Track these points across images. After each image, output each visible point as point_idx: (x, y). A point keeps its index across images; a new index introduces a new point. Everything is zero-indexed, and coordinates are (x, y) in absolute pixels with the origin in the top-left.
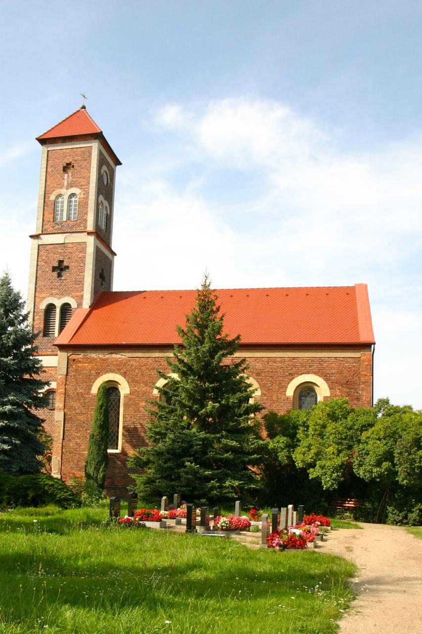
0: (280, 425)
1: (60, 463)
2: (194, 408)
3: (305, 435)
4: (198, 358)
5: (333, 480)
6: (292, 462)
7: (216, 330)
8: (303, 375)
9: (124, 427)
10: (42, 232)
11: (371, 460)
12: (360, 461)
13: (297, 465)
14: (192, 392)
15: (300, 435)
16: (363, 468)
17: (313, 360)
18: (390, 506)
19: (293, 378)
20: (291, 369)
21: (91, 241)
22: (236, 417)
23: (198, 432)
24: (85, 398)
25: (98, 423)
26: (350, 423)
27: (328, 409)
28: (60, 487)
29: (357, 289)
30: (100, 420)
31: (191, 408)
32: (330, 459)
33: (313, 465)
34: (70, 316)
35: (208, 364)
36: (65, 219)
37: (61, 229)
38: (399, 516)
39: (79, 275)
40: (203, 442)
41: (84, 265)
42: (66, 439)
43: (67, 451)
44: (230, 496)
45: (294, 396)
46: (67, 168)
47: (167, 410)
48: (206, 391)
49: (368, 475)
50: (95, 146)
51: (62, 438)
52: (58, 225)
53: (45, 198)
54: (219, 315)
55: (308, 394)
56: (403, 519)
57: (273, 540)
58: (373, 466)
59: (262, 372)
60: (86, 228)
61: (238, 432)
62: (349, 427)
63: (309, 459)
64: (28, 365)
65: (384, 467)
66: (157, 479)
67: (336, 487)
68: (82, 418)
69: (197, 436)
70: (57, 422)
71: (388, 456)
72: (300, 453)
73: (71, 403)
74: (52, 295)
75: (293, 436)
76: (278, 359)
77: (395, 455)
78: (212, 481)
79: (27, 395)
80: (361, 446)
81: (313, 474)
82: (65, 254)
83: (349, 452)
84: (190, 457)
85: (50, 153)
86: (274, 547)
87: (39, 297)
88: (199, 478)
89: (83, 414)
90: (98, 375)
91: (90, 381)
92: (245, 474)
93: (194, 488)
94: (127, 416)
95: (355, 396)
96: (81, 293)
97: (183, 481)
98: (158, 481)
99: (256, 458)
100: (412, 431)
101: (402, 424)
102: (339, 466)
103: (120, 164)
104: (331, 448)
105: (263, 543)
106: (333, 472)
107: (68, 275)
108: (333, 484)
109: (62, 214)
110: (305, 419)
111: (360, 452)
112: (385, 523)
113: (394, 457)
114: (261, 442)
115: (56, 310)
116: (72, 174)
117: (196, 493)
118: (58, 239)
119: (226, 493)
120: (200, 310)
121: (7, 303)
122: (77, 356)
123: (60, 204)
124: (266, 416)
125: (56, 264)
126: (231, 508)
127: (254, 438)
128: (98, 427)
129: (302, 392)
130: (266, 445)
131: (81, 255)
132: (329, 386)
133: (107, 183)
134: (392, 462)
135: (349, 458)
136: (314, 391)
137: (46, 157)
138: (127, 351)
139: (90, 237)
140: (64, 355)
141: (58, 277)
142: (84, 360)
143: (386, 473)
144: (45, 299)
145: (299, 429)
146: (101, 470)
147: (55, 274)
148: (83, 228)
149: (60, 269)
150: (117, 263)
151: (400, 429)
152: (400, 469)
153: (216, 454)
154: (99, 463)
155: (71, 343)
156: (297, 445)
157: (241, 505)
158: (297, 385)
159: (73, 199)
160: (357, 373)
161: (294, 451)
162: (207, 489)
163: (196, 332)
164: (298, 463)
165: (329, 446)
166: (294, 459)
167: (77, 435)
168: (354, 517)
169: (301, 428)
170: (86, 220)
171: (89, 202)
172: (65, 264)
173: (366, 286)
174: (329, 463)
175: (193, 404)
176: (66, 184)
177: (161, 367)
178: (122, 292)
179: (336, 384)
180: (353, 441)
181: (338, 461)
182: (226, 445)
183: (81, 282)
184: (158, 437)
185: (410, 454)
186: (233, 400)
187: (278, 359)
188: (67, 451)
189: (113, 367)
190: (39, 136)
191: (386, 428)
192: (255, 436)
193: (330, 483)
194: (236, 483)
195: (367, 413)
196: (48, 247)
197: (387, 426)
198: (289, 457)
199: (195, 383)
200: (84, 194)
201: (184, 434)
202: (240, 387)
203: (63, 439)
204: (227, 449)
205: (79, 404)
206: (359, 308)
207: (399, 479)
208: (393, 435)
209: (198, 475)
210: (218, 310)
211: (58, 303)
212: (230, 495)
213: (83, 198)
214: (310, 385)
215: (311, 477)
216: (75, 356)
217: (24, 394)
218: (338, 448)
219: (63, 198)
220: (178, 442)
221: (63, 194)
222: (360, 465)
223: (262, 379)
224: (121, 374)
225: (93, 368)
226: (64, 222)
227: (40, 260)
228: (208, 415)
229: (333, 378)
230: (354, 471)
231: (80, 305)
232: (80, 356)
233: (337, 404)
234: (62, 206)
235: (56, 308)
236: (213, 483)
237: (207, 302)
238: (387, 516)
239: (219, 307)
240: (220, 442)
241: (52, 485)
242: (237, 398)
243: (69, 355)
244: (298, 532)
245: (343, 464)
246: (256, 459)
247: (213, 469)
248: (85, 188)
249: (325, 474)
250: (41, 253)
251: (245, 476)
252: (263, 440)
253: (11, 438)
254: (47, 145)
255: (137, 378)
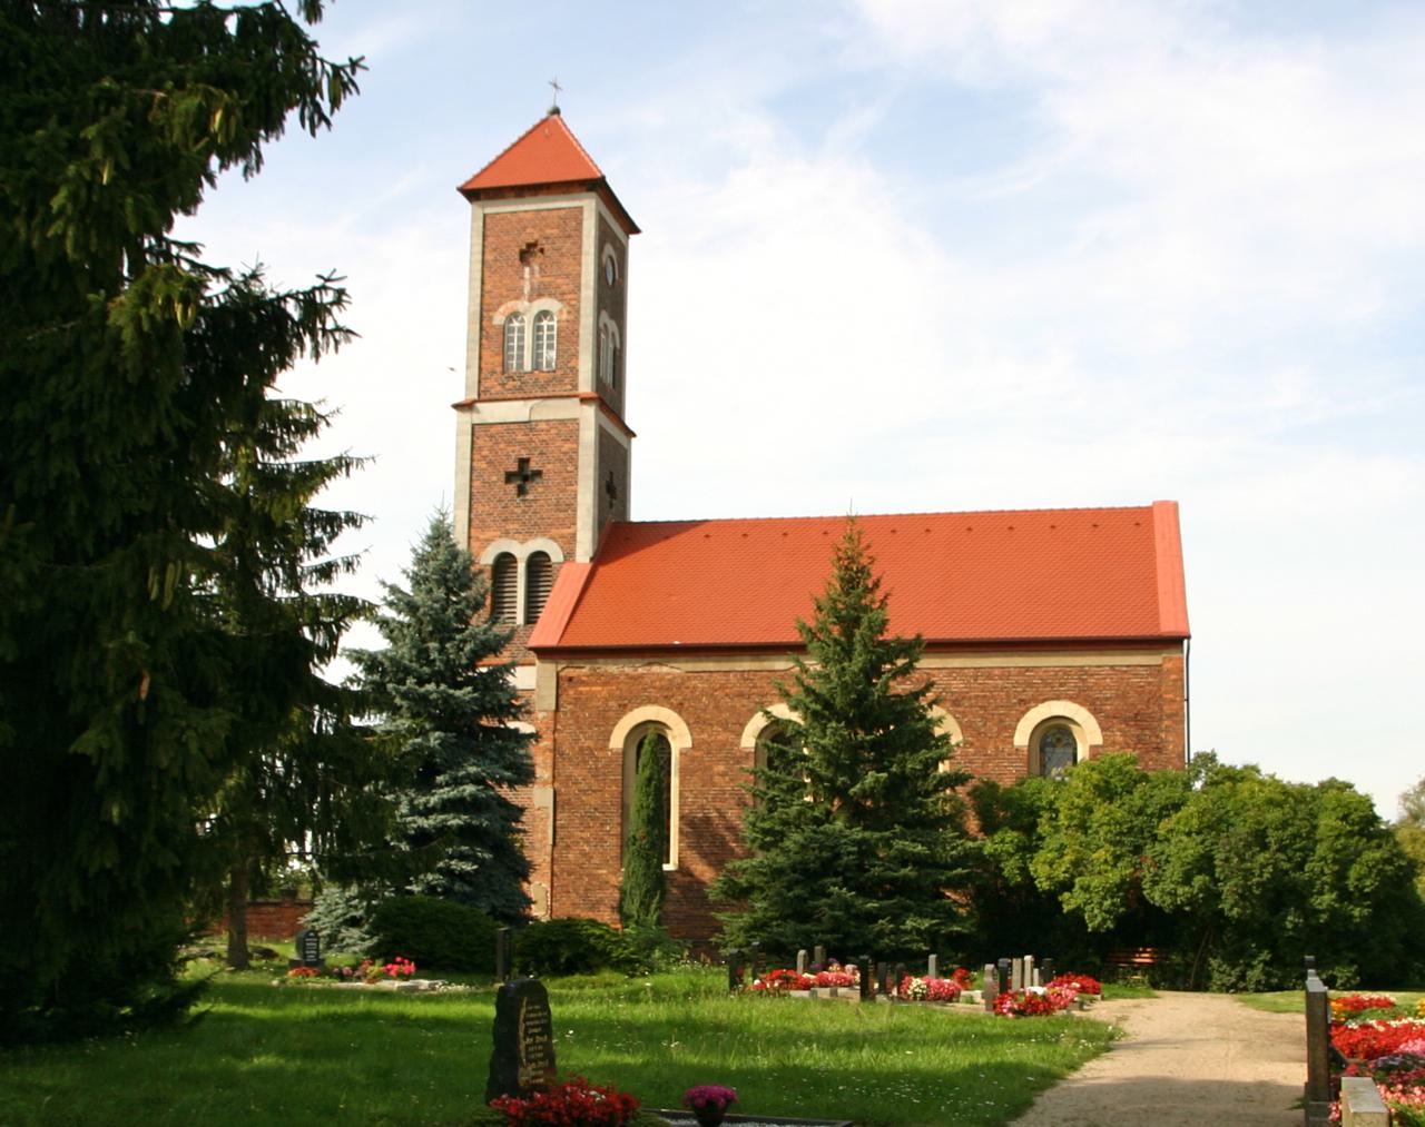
0: (1012, 812)
1: (549, 895)
2: (839, 783)
3: (1054, 827)
4: (845, 686)
5: (1106, 912)
6: (1030, 880)
7: (876, 629)
8: (1046, 704)
9: (682, 818)
10: (479, 395)
11: (1173, 871)
12: (1156, 875)
13: (1039, 886)
14: (834, 751)
15: (1044, 827)
16: (1161, 886)
17: (1067, 671)
18: (1215, 958)
19: (1028, 709)
20: (1024, 691)
21: (588, 417)
22: (920, 799)
23: (847, 828)
24: (597, 759)
25: (644, 813)
26: (1139, 803)
27: (1095, 776)
28: (614, 939)
29: (1157, 516)
30: (648, 807)
31: (832, 781)
32: (1099, 873)
33: (1067, 886)
34: (548, 589)
35: (863, 696)
36: (528, 366)
37: (520, 389)
38: (1230, 975)
39: (564, 491)
40: (859, 848)
41: (577, 469)
42: (561, 844)
43: (563, 871)
44: (915, 948)
45: (1029, 746)
46: (526, 254)
47: (784, 786)
48: (856, 748)
49: (1168, 900)
50: (589, 205)
51: (551, 843)
52: (514, 380)
53: (481, 321)
54: (879, 595)
55: (1059, 740)
56: (1238, 982)
57: (1002, 1004)
58: (1178, 883)
59: (964, 698)
60: (575, 387)
61: (925, 825)
62: (1136, 810)
63: (1060, 873)
64: (500, 701)
65: (1197, 886)
66: (772, 919)
67: (1111, 926)
68: (592, 800)
69: (846, 837)
70: (539, 809)
71: (1205, 863)
72: (1044, 862)
73: (568, 769)
74: (507, 534)
75: (1030, 829)
76: (996, 672)
77: (1216, 862)
78: (880, 921)
79: (497, 762)
80: (1158, 847)
81: (1069, 902)
82: (533, 445)
83: (1136, 859)
84: (837, 877)
85: (488, 220)
86: (1005, 1014)
87: (478, 539)
88: (857, 917)
89: (594, 791)
90: (624, 709)
91: (607, 722)
92: (940, 906)
93: (847, 935)
94: (687, 794)
95: (1152, 743)
96: (570, 531)
97: (826, 923)
98: (775, 923)
99: (961, 874)
100: (1251, 817)
101: (1236, 802)
102: (1117, 886)
103: (636, 230)
104: (1102, 852)
105: (987, 1010)
106: (1104, 898)
107: (540, 490)
108: (1105, 920)
109: (521, 357)
110: (1053, 797)
111: (1157, 859)
112: (1206, 989)
113: (1215, 866)
114: (970, 844)
115: (516, 567)
116: (541, 268)
117: (851, 944)
118: (515, 411)
119: (906, 942)
120: (842, 589)
121: (449, 576)
122: (577, 670)
123: (516, 335)
124: (976, 789)
125: (514, 468)
126: (921, 970)
127: (957, 837)
128: (643, 820)
129: (1045, 737)
130: (980, 849)
131: (567, 447)
132: (1100, 724)
133: (614, 280)
134: (1212, 874)
135: (1136, 870)
136: (1069, 734)
137: (481, 230)
138: (683, 659)
139: (585, 407)
140: (550, 669)
141: (519, 495)
142: (593, 679)
143: (1201, 895)
144: (493, 543)
145: (1040, 817)
146: (653, 906)
147: (512, 488)
148: (569, 387)
149: (523, 476)
150: (638, 450)
151: (1232, 813)
152: (1226, 889)
153: (886, 870)
154: (649, 894)
155: (565, 644)
156: (1037, 846)
157: (939, 962)
158: (1036, 723)
159: (545, 323)
160: (1155, 697)
161: (1032, 858)
162: (871, 937)
163: (836, 631)
164: (1040, 882)
165: (1099, 848)
166: (1032, 873)
167: (583, 835)
168: (1150, 982)
169: (1046, 815)
170: (575, 371)
171: (581, 332)
172: (533, 466)
173: (1175, 506)
174: (1096, 882)
175: (835, 775)
176: (527, 290)
177: (754, 690)
178: (656, 523)
179: (1115, 721)
180: (1144, 838)
181: (1114, 877)
182: (902, 852)
183: (571, 506)
184: (768, 839)
185: (1243, 860)
186: (913, 764)
187: (996, 672)
188: (563, 871)
189: (653, 693)
190: (469, 177)
191: (1202, 813)
192: (957, 834)
193: (1099, 919)
194: (926, 924)
195: (1172, 782)
196: (493, 430)
197: (1205, 810)
198: (1024, 870)
199: (841, 735)
200: (569, 312)
201: (822, 833)
202: (925, 739)
203: (554, 844)
204: (904, 859)
205: (584, 772)
206: (1159, 559)
207: (1225, 906)
208: (1215, 824)
209: (853, 911)
210: (876, 585)
211: (522, 551)
212: (914, 946)
213: (568, 321)
214: (1063, 722)
215: (1066, 908)
216: (572, 670)
217: (491, 759)
218: (1115, 851)
219: (523, 321)
220: (814, 849)
221: (521, 311)
222: (1155, 883)
223: (964, 712)
224: (672, 707)
225: (611, 696)
226: (526, 373)
227: (476, 457)
228: (865, 795)
229: (1108, 707)
230: (1145, 893)
231: (569, 556)
232: (584, 670)
233: (1112, 767)
234: (521, 339)
235: (516, 562)
236: (882, 924)
237: (854, 557)
238: (1210, 978)
239: (879, 581)
240: (891, 847)
241: (601, 937)
242: (920, 761)
243: (559, 668)
244: (1040, 991)
245: (1123, 881)
246: (961, 876)
247: (879, 899)
248: (570, 297)
249: (1090, 902)
250: (480, 442)
251: (941, 910)
252: (975, 840)
253: (473, 850)
254: (480, 203)
255: (706, 714)
